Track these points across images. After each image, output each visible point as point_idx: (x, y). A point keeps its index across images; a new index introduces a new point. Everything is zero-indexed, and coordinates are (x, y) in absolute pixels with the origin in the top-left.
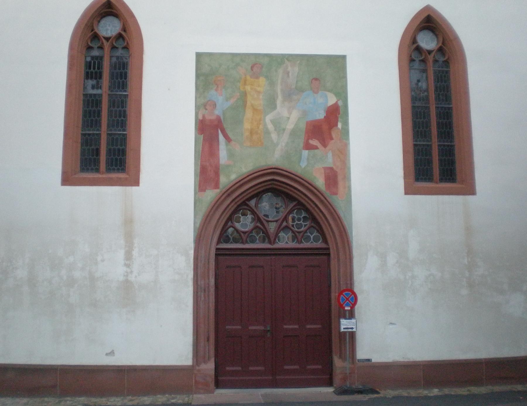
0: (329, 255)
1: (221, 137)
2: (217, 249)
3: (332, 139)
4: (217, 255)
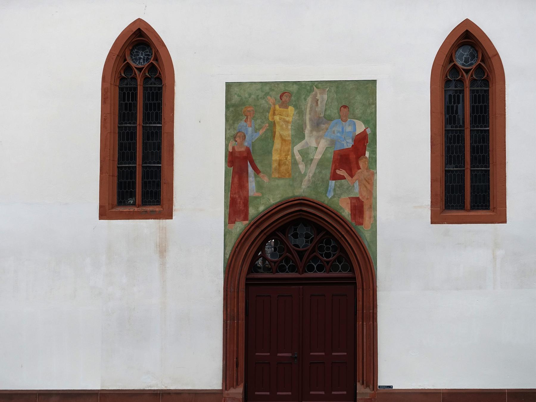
0: (355, 284)
2: (247, 279)
3: (359, 168)
4: (247, 285)
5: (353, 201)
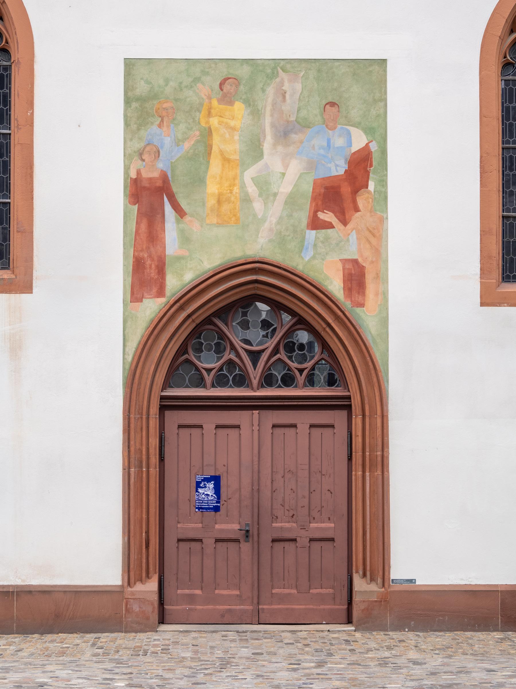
0: (349, 408)
1: (168, 208)
3: (357, 209)
5: (349, 266)
